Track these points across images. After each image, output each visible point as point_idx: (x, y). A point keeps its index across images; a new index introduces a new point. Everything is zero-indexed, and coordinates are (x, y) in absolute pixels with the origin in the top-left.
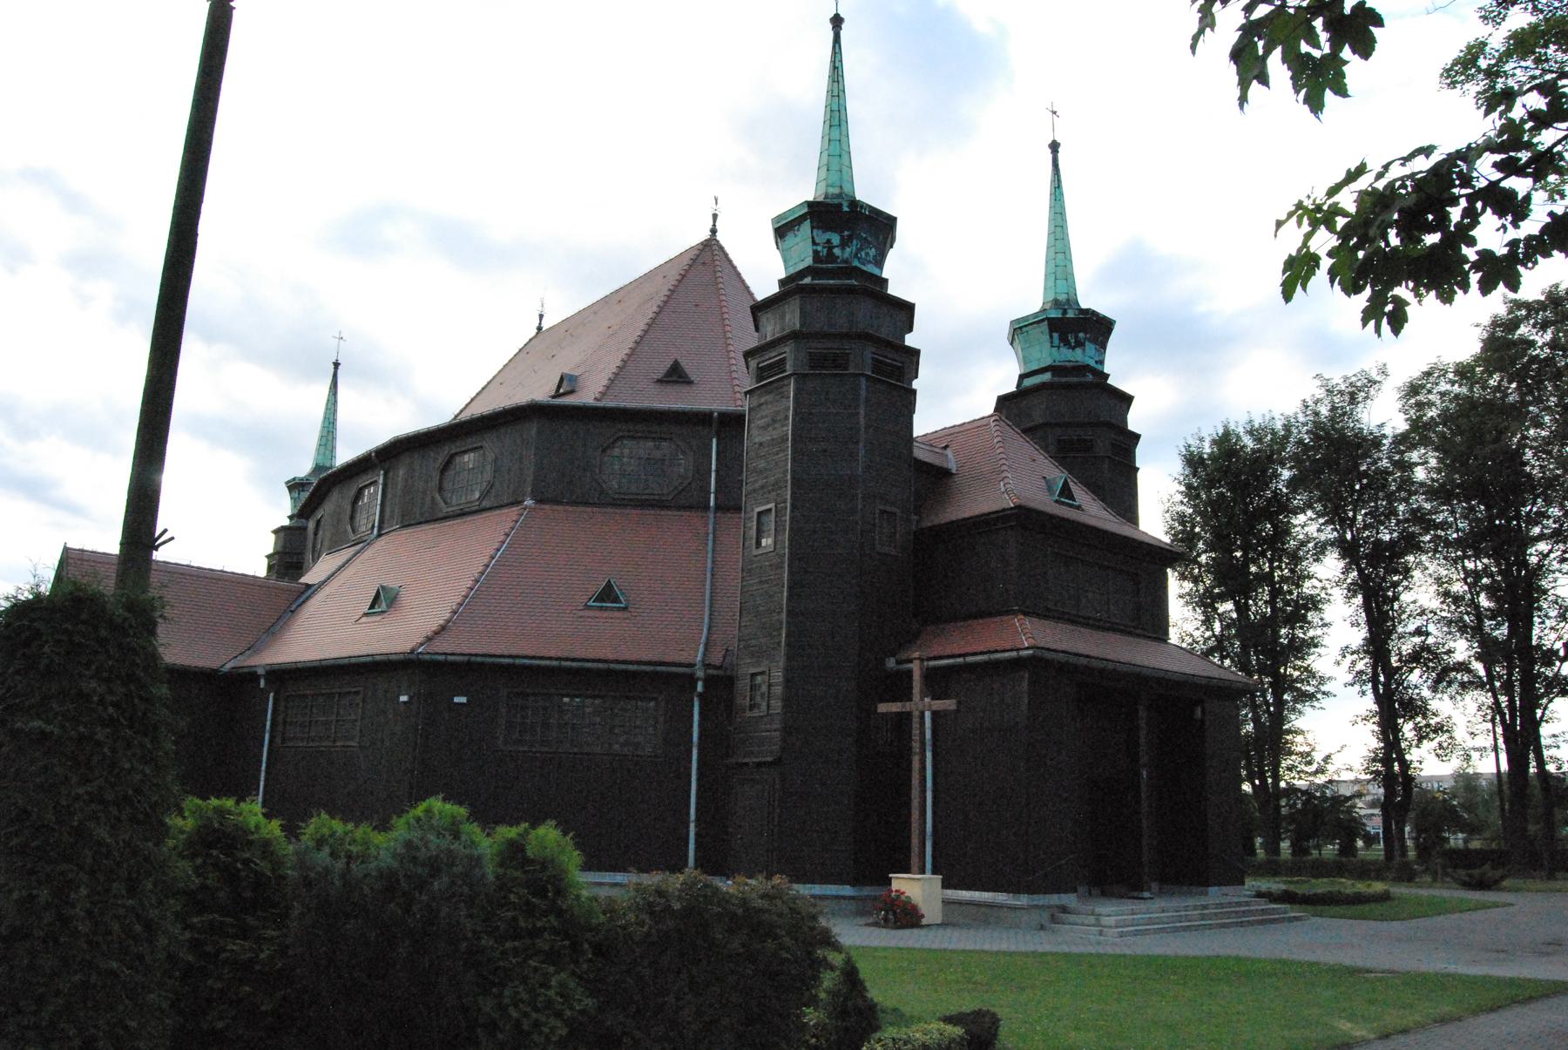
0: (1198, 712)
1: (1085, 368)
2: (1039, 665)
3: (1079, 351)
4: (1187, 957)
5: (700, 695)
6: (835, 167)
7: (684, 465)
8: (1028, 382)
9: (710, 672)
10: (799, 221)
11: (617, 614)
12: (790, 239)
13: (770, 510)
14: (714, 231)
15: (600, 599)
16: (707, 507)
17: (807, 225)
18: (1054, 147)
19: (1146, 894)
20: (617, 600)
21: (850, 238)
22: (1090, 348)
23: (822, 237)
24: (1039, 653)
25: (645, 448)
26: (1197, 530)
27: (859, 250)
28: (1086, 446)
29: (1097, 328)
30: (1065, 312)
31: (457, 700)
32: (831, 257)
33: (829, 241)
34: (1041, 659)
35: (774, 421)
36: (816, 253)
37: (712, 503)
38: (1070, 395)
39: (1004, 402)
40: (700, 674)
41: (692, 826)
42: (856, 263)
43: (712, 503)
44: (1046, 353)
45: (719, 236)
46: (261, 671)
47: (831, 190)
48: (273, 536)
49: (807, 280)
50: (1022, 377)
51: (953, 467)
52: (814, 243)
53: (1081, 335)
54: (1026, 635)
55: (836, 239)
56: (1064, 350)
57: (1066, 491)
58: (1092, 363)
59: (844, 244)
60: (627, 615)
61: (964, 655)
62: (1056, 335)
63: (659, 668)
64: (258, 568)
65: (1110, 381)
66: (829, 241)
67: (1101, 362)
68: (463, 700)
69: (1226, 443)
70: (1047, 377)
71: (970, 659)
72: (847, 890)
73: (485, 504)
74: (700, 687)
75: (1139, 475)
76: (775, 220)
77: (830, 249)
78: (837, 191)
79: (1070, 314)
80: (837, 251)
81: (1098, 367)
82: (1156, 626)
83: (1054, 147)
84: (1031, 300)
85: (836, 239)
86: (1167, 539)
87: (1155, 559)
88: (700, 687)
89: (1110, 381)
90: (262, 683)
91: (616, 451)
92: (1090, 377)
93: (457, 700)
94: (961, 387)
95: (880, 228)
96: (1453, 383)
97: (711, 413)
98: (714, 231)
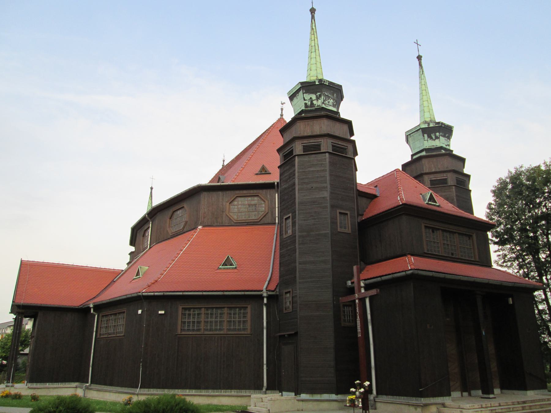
1: (441, 148)
2: (415, 279)
3: (437, 140)
5: (266, 304)
6: (313, 67)
7: (263, 208)
8: (415, 157)
9: (269, 293)
10: (298, 91)
11: (233, 271)
12: (295, 100)
13: (289, 217)
14: (282, 115)
15: (225, 264)
16: (275, 224)
17: (301, 92)
19: (491, 396)
20: (231, 265)
21: (320, 96)
23: (307, 96)
24: (416, 272)
25: (246, 201)
27: (324, 101)
28: (444, 181)
31: (160, 312)
33: (311, 98)
34: (418, 275)
35: (290, 177)
36: (306, 104)
37: (277, 222)
38: (436, 162)
39: (405, 166)
41: (265, 367)
42: (323, 106)
43: (277, 222)
45: (284, 117)
46: (91, 306)
48: (129, 256)
50: (412, 156)
51: (377, 194)
52: (305, 100)
53: (437, 134)
54: (411, 263)
56: (430, 141)
57: (431, 198)
58: (444, 146)
59: (318, 98)
60: (236, 271)
62: (426, 135)
64: (124, 267)
65: (454, 153)
66: (311, 98)
67: (449, 145)
68: (163, 312)
69: (515, 178)
72: (333, 397)
73: (185, 230)
74: (265, 301)
75: (472, 194)
76: (288, 93)
79: (431, 125)
80: (315, 102)
81: (447, 147)
82: (487, 263)
85: (314, 97)
86: (485, 219)
87: (483, 227)
88: (265, 301)
91: (235, 203)
92: (443, 151)
93: (160, 312)
94: (379, 155)
97: (274, 183)
98: (282, 115)
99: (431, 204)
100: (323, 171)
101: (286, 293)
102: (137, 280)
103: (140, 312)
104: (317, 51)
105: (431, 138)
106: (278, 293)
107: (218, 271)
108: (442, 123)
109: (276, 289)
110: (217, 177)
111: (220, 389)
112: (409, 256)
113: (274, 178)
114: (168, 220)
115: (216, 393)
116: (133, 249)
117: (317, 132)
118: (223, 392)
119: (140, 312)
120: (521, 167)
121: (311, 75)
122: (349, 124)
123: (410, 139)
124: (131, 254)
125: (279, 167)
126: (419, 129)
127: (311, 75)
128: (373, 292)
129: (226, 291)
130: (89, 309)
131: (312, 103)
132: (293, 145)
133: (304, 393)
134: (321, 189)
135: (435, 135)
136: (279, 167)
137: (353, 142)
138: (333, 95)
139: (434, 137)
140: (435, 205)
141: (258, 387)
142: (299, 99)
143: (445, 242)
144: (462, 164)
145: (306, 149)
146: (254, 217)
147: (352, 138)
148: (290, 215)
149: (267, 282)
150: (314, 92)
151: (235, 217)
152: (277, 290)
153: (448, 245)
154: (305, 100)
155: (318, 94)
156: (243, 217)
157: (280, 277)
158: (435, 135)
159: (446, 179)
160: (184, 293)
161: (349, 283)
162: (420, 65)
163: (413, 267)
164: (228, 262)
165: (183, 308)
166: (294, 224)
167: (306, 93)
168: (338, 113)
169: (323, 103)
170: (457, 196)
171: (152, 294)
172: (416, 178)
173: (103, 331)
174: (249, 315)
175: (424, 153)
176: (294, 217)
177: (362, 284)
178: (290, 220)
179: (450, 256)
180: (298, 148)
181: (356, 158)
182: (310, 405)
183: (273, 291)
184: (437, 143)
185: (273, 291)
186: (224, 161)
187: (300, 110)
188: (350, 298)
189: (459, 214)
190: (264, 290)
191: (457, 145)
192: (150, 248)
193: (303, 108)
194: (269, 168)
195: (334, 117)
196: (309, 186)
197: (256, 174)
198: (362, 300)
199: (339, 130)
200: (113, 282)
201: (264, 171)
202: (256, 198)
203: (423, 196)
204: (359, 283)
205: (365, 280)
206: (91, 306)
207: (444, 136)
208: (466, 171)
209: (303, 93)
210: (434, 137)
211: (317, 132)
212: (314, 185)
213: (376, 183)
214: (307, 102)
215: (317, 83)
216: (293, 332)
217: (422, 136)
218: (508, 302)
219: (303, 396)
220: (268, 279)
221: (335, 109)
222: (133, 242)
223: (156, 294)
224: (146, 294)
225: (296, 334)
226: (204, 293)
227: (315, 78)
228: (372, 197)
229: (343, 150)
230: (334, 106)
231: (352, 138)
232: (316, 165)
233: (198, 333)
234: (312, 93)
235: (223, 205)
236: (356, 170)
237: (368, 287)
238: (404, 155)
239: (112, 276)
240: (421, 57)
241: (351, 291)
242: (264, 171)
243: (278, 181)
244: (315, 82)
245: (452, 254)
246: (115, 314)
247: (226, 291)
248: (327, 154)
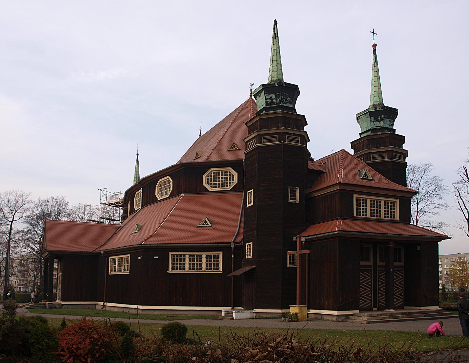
0: (419, 248)
1: (385, 128)
3: (382, 122)
4: (354, 331)
8: (362, 136)
11: (209, 228)
18: (374, 46)
21: (279, 95)
22: (387, 121)
24: (340, 232)
27: (282, 99)
29: (392, 113)
30: (376, 109)
32: (272, 103)
33: (271, 97)
36: (266, 102)
40: (232, 246)
42: (282, 104)
44: (369, 125)
47: (273, 79)
49: (264, 112)
52: (266, 99)
55: (274, 96)
58: (388, 126)
60: (211, 228)
61: (316, 235)
62: (372, 118)
63: (318, 236)
65: (397, 133)
66: (271, 97)
70: (370, 133)
71: (318, 236)
78: (275, 79)
79: (378, 109)
83: (374, 46)
84: (365, 104)
85: (274, 96)
95: (293, 91)
104: (278, 54)
107: (197, 229)
109: (241, 242)
117: (277, 105)
123: (359, 120)
135: (381, 117)
142: (261, 98)
158: (381, 117)
162: (375, 52)
169: (281, 101)
183: (240, 243)
185: (240, 243)
186: (201, 131)
187: (262, 107)
189: (171, 323)
191: (399, 127)
192: (142, 208)
200: (115, 233)
203: (360, 173)
209: (265, 94)
210: (379, 119)
211: (277, 105)
214: (268, 100)
215: (276, 85)
238: (355, 132)
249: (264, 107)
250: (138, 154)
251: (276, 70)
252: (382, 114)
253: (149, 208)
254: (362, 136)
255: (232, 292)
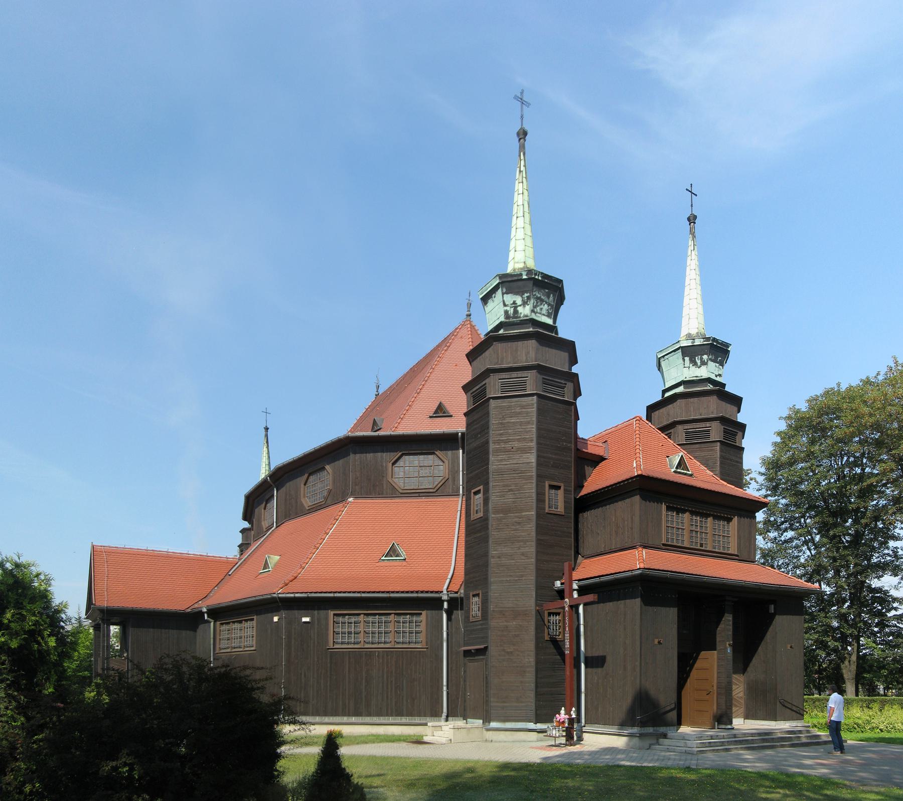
1: (709, 380)
3: (703, 367)
8: (667, 395)
11: (400, 563)
17: (499, 291)
23: (509, 299)
26: (868, 470)
27: (535, 307)
33: (514, 303)
34: (647, 575)
36: (506, 312)
40: (445, 597)
42: (534, 316)
46: (205, 610)
49: (501, 332)
51: (606, 455)
52: (505, 305)
53: (705, 357)
55: (519, 301)
56: (693, 368)
59: (524, 303)
60: (404, 563)
62: (687, 359)
65: (726, 389)
66: (514, 303)
72: (531, 725)
74: (446, 605)
77: (515, 308)
79: (697, 342)
80: (520, 309)
81: (718, 379)
85: (519, 301)
88: (446, 605)
89: (726, 389)
90: (206, 615)
94: (610, 407)
96: (69, 667)
99: (680, 473)
100: (528, 423)
101: (474, 596)
102: (265, 574)
103: (276, 619)
105: (695, 364)
106: (462, 595)
107: (377, 564)
108: (714, 340)
110: (371, 415)
111: (387, 715)
112: (640, 549)
113: (457, 425)
114: (302, 485)
115: (382, 720)
116: (246, 525)
118: (391, 720)
119: (276, 619)
120: (878, 374)
121: (516, 260)
122: (569, 347)
124: (243, 531)
125: (465, 414)
126: (678, 349)
127: (516, 260)
128: (591, 597)
129: (393, 592)
130: (202, 613)
131: (516, 312)
132: (487, 381)
133: (494, 721)
134: (524, 451)
135: (701, 359)
136: (465, 414)
137: (576, 376)
138: (549, 297)
139: (699, 362)
140: (685, 474)
141: (435, 713)
143: (694, 528)
144: (736, 409)
145: (505, 387)
146: (427, 484)
147: (575, 369)
148: (481, 487)
149: (448, 581)
150: (520, 293)
151: (402, 485)
152: (462, 591)
153: (697, 532)
154: (505, 305)
155: (526, 295)
156: (412, 484)
157: (466, 574)
158: (701, 359)
159: (709, 431)
160: (336, 595)
161: (558, 584)
163: (642, 566)
164: (393, 552)
165: (334, 615)
166: (486, 501)
167: (507, 293)
168: (553, 329)
169: (533, 311)
170: (721, 457)
171: (292, 595)
172: (663, 429)
173: (224, 644)
174: (423, 624)
175: (681, 389)
176: (486, 491)
177: (575, 586)
178: (480, 495)
179: (699, 547)
180: (494, 387)
181: (579, 402)
182: (502, 736)
183: (457, 593)
184: (703, 372)
185: (457, 593)
186: (378, 387)
187: (497, 322)
188: (558, 603)
190: (445, 592)
193: (502, 319)
194: (449, 407)
195: (546, 336)
196: (508, 446)
197: (431, 417)
198: (574, 607)
199: (555, 359)
201: (441, 411)
202: (431, 457)
204: (571, 585)
205: (579, 580)
206: (205, 610)
207: (714, 361)
208: (741, 418)
209: (503, 294)
210: (699, 362)
212: (516, 444)
213: (604, 439)
214: (508, 308)
215: (525, 277)
216: (482, 647)
217: (681, 361)
218: (768, 609)
219: (494, 724)
220: (450, 576)
221: (550, 321)
222: (247, 515)
223: (297, 595)
224: (284, 595)
225: (486, 648)
226: (363, 595)
227: (521, 265)
228: (597, 460)
229: (559, 387)
230: (549, 316)
231: (575, 369)
232: (520, 413)
233: (356, 646)
234: (516, 293)
235: (382, 466)
236: (577, 418)
237: (582, 591)
239: (224, 570)
240: (695, 217)
241: (561, 594)
242: (441, 411)
243: (464, 430)
244: (521, 275)
245: (701, 545)
246: (240, 622)
247: (393, 592)
248: (535, 397)
249: (501, 322)
250: (267, 429)
251: (522, 247)
252: (602, 459)
253: (289, 526)
254: (667, 395)
255: (445, 683)
